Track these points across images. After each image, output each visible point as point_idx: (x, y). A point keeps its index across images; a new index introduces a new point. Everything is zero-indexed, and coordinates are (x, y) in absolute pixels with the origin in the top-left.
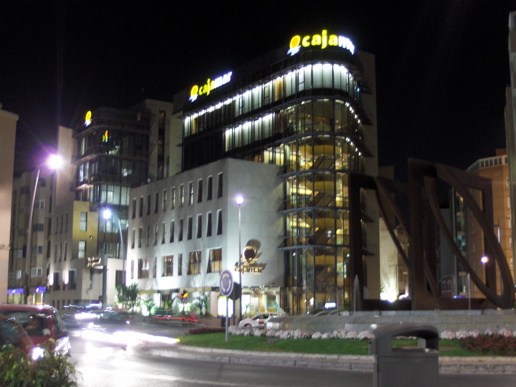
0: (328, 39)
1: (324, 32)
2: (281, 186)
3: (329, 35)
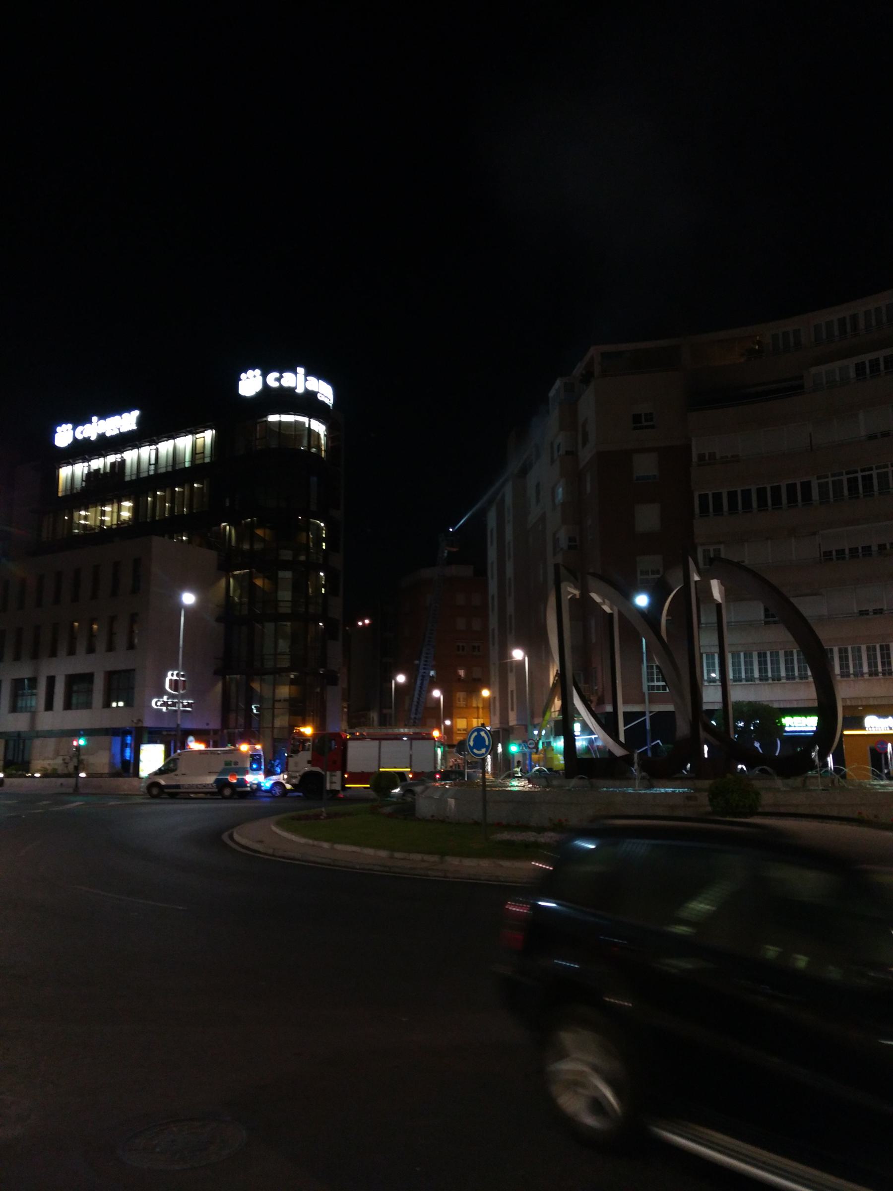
0: (306, 380)
1: (301, 370)
2: (223, 582)
3: (307, 374)
